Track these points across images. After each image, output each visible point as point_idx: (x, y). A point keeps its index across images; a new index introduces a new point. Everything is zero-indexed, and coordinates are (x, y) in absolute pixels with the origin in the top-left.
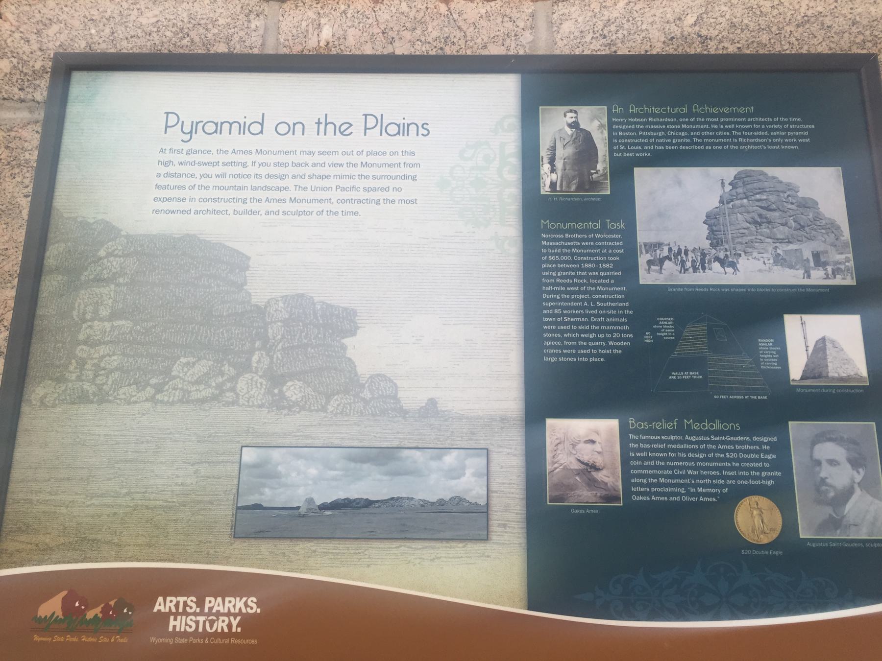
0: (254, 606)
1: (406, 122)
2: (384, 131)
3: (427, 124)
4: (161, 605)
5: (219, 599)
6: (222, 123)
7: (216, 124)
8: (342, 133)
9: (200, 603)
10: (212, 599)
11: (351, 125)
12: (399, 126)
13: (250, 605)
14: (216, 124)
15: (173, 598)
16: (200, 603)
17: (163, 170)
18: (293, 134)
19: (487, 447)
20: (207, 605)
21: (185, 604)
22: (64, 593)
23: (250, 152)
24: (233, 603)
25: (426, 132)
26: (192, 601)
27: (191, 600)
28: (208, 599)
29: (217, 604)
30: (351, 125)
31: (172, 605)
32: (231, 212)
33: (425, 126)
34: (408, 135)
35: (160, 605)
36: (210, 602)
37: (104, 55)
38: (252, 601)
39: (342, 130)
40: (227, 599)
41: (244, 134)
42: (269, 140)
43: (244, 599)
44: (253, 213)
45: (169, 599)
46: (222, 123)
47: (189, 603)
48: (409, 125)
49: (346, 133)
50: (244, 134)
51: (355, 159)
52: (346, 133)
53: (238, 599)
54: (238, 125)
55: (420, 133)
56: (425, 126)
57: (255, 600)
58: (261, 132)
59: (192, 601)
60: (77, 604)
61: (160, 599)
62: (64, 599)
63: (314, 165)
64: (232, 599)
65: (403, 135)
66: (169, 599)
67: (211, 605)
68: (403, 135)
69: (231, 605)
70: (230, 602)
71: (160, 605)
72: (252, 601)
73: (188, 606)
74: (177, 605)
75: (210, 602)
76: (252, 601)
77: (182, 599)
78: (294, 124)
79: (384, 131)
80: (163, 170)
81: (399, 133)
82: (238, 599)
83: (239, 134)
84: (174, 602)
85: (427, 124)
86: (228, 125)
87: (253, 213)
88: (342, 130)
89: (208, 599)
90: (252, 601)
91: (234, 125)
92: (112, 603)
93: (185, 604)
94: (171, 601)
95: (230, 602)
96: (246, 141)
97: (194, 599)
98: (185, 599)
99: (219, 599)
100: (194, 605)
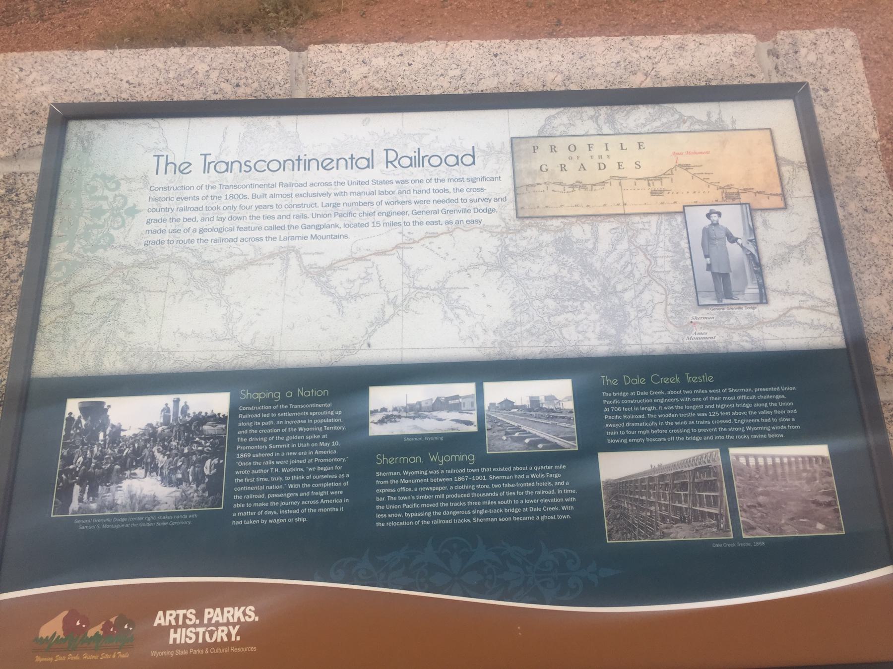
1: (308, 158)
2: (320, 167)
3: (250, 162)
5: (218, 610)
6: (232, 163)
7: (227, 164)
8: (324, 168)
10: (211, 610)
11: (190, 164)
12: (411, 159)
14: (227, 164)
15: (173, 612)
17: (154, 205)
18: (284, 170)
19: (788, 207)
22: (65, 613)
24: (231, 613)
26: (191, 613)
27: (191, 613)
28: (207, 610)
29: (216, 613)
30: (190, 164)
33: (248, 163)
34: (309, 169)
36: (209, 613)
37: (142, 104)
38: (250, 610)
39: (324, 165)
40: (226, 609)
41: (352, 168)
42: (379, 172)
43: (242, 608)
44: (362, 225)
45: (168, 612)
46: (232, 163)
48: (309, 161)
49: (185, 171)
50: (352, 168)
52: (185, 171)
53: (236, 608)
54: (173, 166)
55: (242, 170)
56: (248, 163)
57: (253, 608)
58: (474, 163)
59: (191, 613)
64: (231, 609)
65: (419, 166)
66: (168, 612)
68: (419, 166)
70: (229, 612)
72: (250, 610)
75: (209, 613)
76: (250, 610)
77: (181, 612)
78: (285, 161)
79: (320, 167)
80: (154, 205)
81: (411, 165)
82: (236, 608)
83: (204, 172)
85: (250, 162)
87: (362, 225)
88: (181, 169)
89: (207, 610)
90: (250, 610)
95: (229, 612)
96: (354, 175)
97: (194, 611)
98: (184, 611)
99: (218, 610)
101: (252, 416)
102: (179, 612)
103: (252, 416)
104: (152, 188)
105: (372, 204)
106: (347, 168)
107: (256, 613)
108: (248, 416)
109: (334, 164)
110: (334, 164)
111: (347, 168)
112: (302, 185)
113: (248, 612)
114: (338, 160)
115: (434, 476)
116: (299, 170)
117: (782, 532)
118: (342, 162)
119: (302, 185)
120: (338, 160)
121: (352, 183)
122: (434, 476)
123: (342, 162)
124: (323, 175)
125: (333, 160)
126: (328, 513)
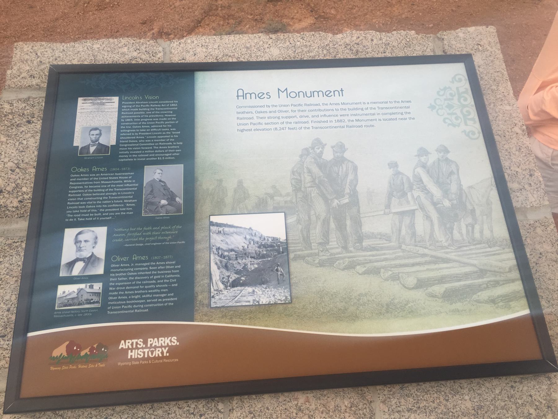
0: (176, 341)
4: (123, 345)
5: (156, 339)
6: (311, 96)
8: (259, 98)
9: (145, 342)
10: (152, 339)
13: (174, 341)
15: (130, 341)
16: (145, 342)
20: (149, 343)
21: (137, 343)
23: (339, 104)
25: (269, 97)
26: (140, 341)
27: (140, 341)
28: (149, 340)
29: (155, 341)
31: (129, 344)
32: (310, 122)
33: (268, 94)
34: (246, 99)
35: (122, 345)
36: (151, 341)
38: (174, 339)
39: (259, 96)
40: (160, 339)
43: (170, 338)
47: (139, 342)
48: (311, 96)
49: (329, 95)
51: (339, 107)
52: (329, 95)
53: (166, 338)
56: (268, 94)
57: (176, 338)
59: (140, 341)
60: (75, 348)
61: (123, 342)
62: (67, 346)
63: (270, 112)
64: (163, 339)
67: (151, 343)
69: (162, 342)
70: (162, 340)
71: (122, 345)
72: (174, 339)
73: (138, 344)
74: (132, 344)
75: (151, 341)
76: (174, 339)
77: (135, 341)
78: (299, 93)
84: (131, 343)
86: (249, 95)
88: (259, 96)
89: (149, 340)
90: (174, 339)
91: (252, 95)
92: (95, 346)
93: (137, 343)
94: (129, 342)
96: (258, 102)
97: (142, 340)
98: (136, 340)
99: (156, 339)
100: (142, 344)
101: (76, 195)
102: (133, 341)
103: (76, 195)
104: (238, 107)
105: (252, 113)
106: (339, 96)
107: (178, 340)
108: (74, 195)
109: (332, 93)
110: (332, 93)
111: (339, 96)
112: (317, 105)
113: (173, 340)
114: (334, 92)
115: (117, 212)
116: (343, 96)
117: (158, 212)
118: (336, 93)
119: (317, 105)
120: (334, 92)
121: (281, 106)
122: (117, 212)
123: (336, 93)
124: (326, 100)
125: (331, 92)
126: (129, 247)
